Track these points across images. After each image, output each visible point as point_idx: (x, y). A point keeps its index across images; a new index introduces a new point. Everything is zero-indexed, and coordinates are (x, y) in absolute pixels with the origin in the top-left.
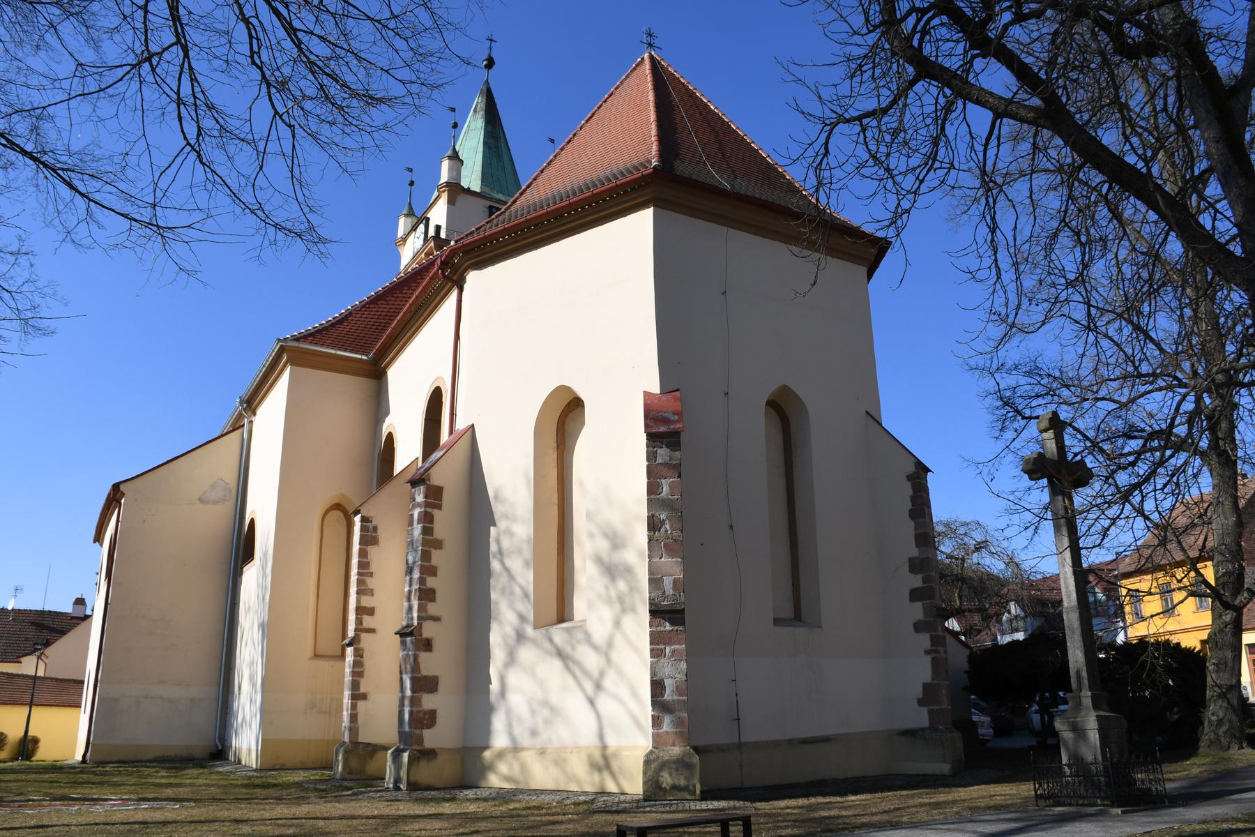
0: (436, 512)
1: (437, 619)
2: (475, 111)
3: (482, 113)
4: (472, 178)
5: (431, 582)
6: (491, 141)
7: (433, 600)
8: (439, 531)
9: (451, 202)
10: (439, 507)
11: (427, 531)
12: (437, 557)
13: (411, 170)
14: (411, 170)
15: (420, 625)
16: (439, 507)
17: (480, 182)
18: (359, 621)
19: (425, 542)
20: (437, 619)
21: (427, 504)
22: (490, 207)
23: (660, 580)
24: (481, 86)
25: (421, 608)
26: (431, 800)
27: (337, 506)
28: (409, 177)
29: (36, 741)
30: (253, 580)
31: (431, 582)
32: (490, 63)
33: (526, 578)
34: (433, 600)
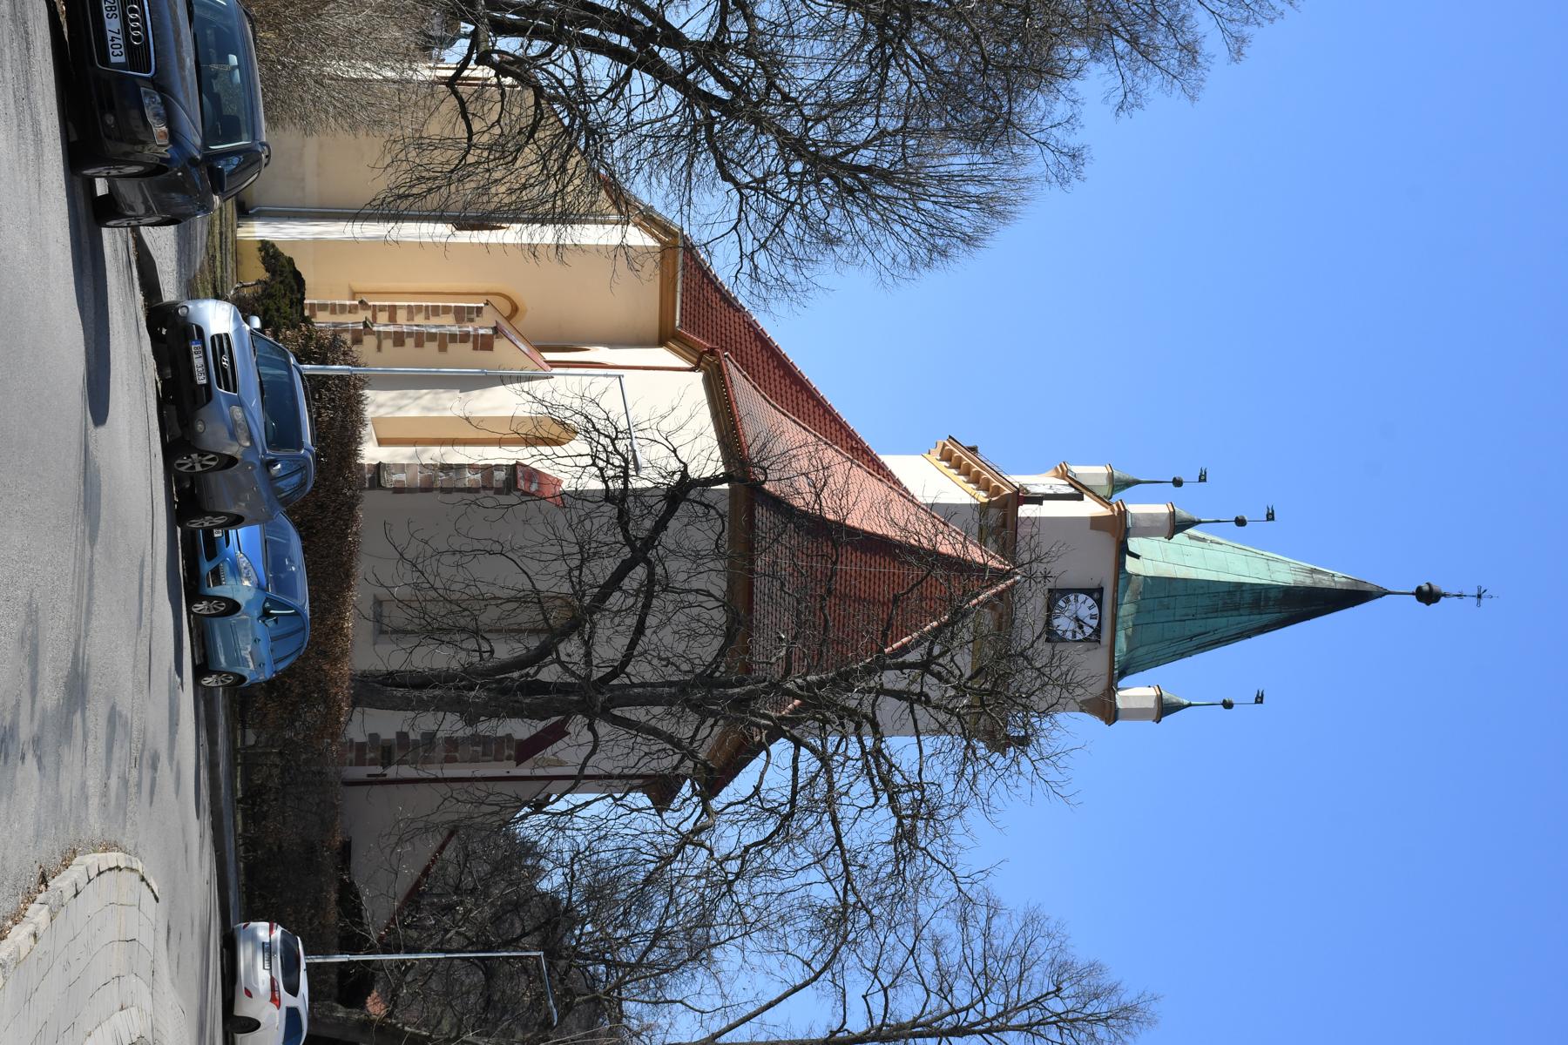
0: (470, 345)
1: (379, 348)
2: (1313, 571)
3: (1308, 582)
4: (1153, 558)
5: (410, 342)
6: (1248, 597)
7: (395, 345)
8: (455, 349)
9: (1096, 523)
10: (475, 348)
11: (453, 338)
12: (431, 347)
13: (1202, 478)
14: (1202, 478)
15: (373, 333)
16: (475, 348)
17: (1151, 573)
18: (382, 308)
19: (443, 335)
20: (379, 348)
21: (476, 336)
22: (1100, 590)
23: (403, 471)
24: (1374, 580)
25: (387, 334)
26: (212, 742)
27: (515, 309)
28: (1189, 476)
29: (1419, 589)
30: (442, 230)
31: (410, 342)
32: (1428, 596)
33: (413, 412)
34: (395, 345)
